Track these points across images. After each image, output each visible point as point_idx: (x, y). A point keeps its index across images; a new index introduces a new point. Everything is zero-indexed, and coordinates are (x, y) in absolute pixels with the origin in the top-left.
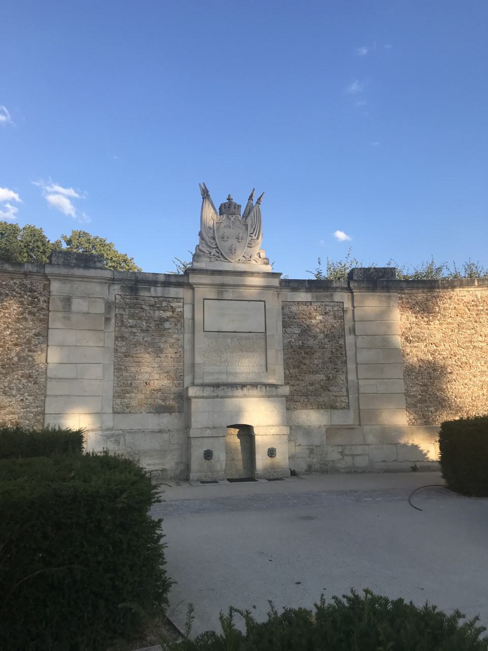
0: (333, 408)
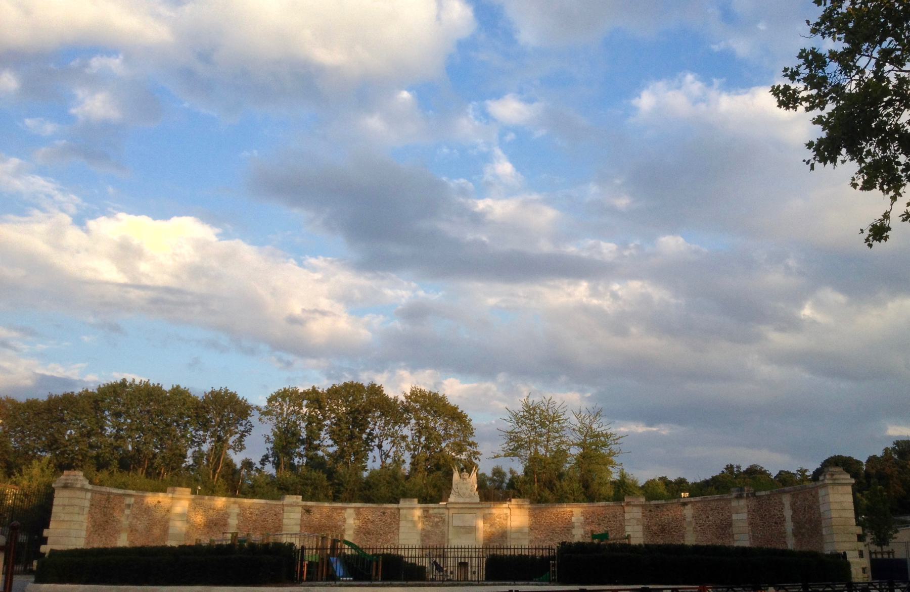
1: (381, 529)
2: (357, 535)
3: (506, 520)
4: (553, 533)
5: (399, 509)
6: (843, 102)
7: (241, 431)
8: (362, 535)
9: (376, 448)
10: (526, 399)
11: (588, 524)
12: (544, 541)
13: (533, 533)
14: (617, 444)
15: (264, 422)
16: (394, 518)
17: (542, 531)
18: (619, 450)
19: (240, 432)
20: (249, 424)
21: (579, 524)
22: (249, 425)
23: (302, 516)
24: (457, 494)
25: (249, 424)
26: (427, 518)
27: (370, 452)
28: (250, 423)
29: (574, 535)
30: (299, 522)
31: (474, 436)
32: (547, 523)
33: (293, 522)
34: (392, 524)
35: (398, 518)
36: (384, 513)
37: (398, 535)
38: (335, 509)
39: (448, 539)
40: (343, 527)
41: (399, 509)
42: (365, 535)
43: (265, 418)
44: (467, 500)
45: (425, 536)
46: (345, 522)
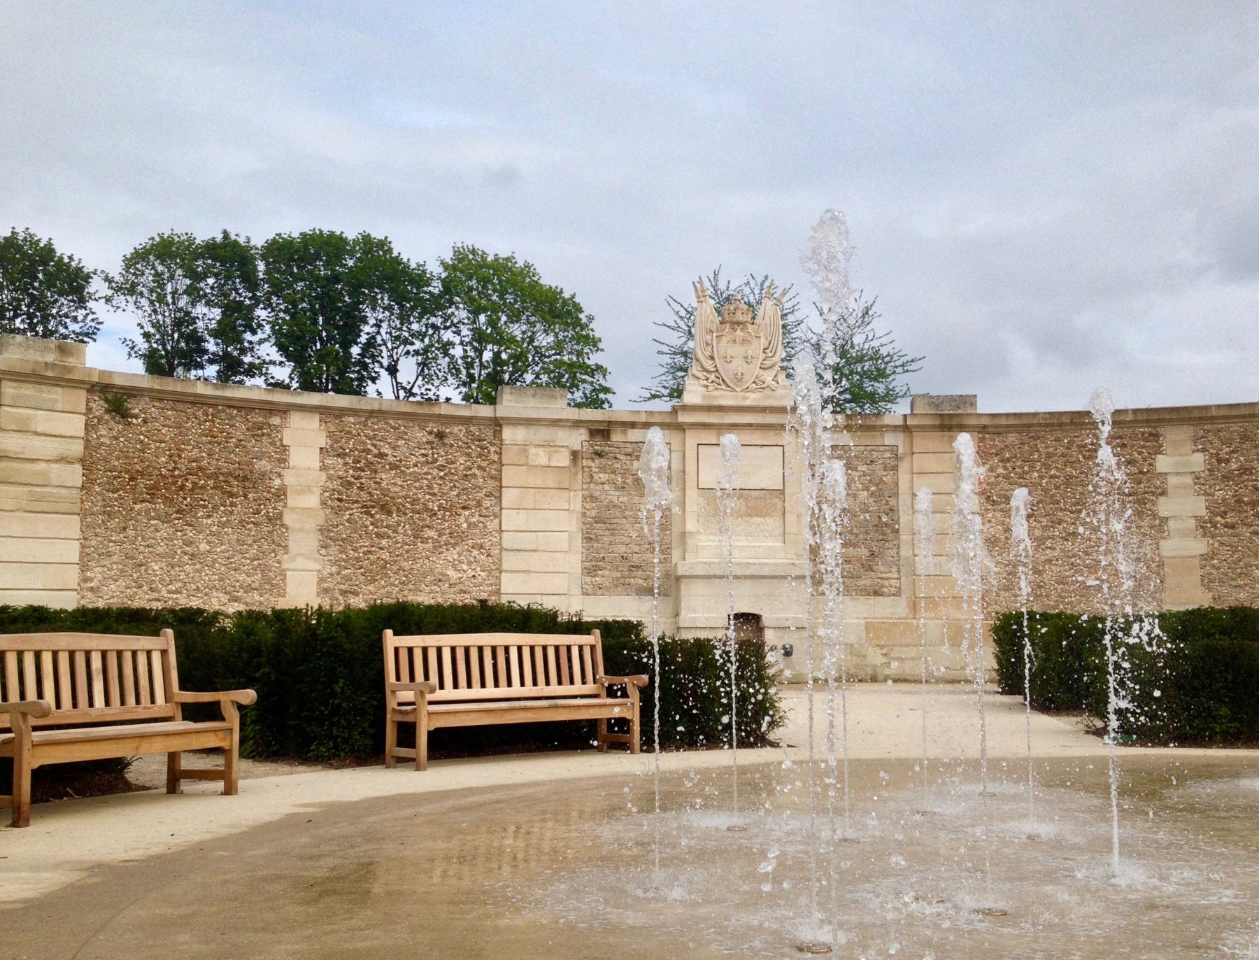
0: (876, 593)
1: (434, 495)
2: (338, 511)
3: (895, 468)
5: (497, 424)
6: (248, 696)
7: (74, 332)
8: (356, 512)
9: (384, 373)
10: (712, 279)
11: (1226, 478)
13: (999, 515)
14: (907, 371)
15: (118, 307)
16: (480, 455)
18: (905, 388)
19: (73, 336)
20: (91, 317)
21: (1189, 480)
22: (93, 320)
23: (88, 427)
24: (712, 377)
25: (91, 317)
26: (603, 461)
27: (370, 382)
28: (93, 313)
30: (77, 448)
31: (602, 350)
32: (1052, 477)
33: (50, 448)
34: (474, 476)
35: (496, 458)
36: (441, 436)
37: (498, 516)
38: (239, 408)
39: (683, 535)
40: (277, 482)
41: (497, 424)
42: (368, 513)
43: (120, 299)
44: (752, 399)
45: (598, 520)
46: (283, 461)
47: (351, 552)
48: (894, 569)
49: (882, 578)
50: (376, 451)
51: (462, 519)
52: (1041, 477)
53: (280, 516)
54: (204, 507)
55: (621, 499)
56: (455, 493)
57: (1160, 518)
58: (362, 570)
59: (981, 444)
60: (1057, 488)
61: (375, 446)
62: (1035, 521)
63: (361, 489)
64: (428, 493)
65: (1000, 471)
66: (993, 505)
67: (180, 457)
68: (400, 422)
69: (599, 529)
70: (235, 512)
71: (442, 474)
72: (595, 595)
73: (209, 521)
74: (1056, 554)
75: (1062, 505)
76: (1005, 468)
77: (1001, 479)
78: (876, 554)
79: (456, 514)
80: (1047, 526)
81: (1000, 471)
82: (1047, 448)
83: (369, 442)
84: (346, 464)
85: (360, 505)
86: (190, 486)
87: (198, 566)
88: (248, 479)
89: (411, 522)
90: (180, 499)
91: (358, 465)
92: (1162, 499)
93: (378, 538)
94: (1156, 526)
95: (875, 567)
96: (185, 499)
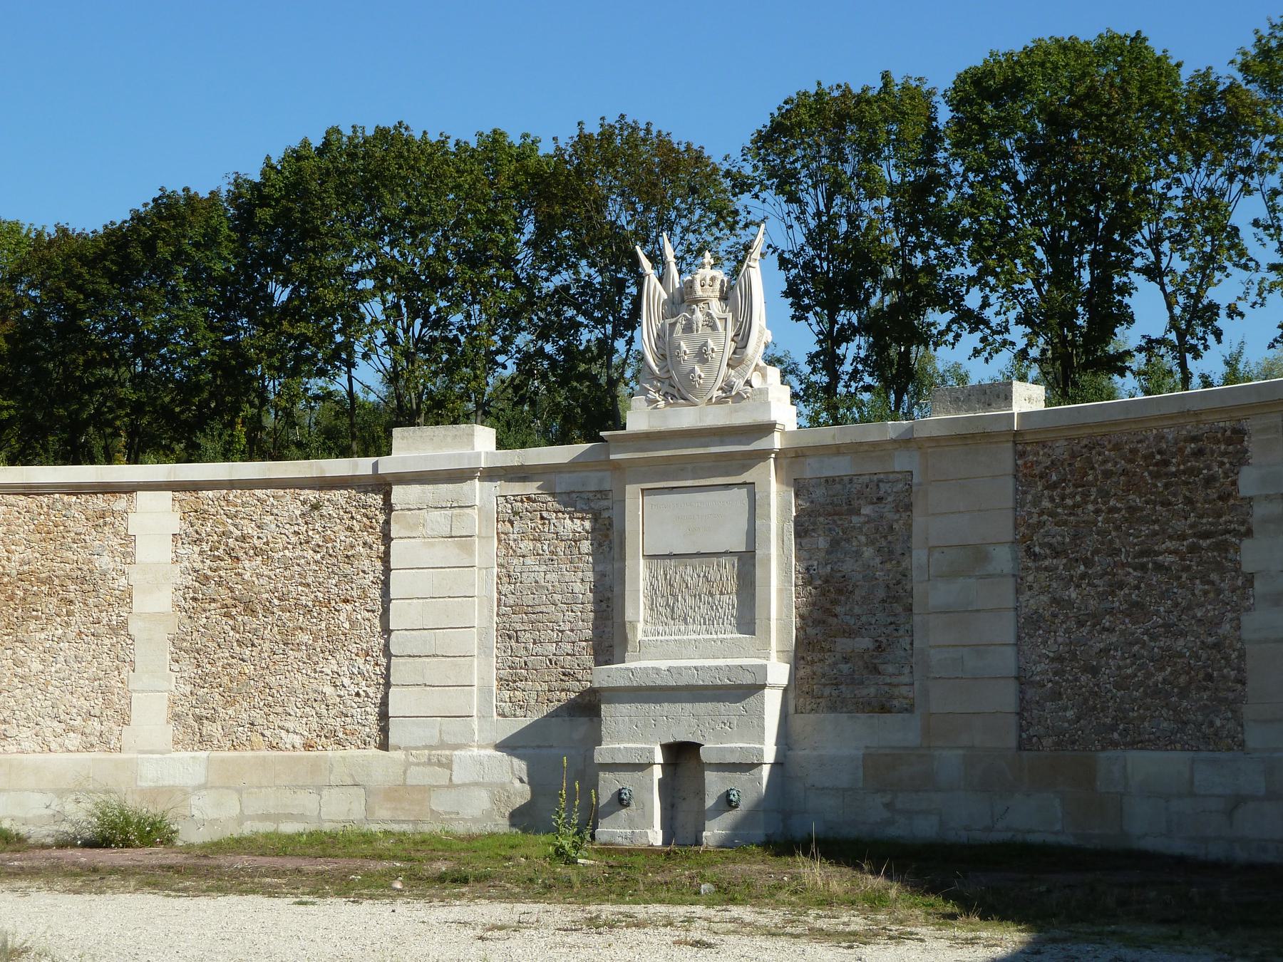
0: (884, 709)
1: (308, 585)
3: (909, 507)
4: (1143, 567)
5: (382, 485)
12: (1096, 618)
17: (1088, 563)
29: (1250, 579)
32: (1113, 510)
41: (382, 485)
42: (227, 615)
47: (208, 666)
48: (906, 670)
49: (890, 684)
50: (239, 533)
51: (343, 616)
52: (1097, 512)
53: (124, 625)
54: (37, 618)
55: (548, 577)
56: (334, 582)
57: (1245, 575)
58: (221, 689)
59: (1019, 462)
60: (1118, 528)
61: (235, 526)
62: (1089, 584)
63: (219, 584)
64: (301, 584)
65: (1046, 504)
66: (1034, 561)
67: (9, 559)
68: (268, 492)
69: (517, 621)
70: (73, 622)
71: (318, 557)
72: (515, 716)
73: (43, 636)
74: (1114, 639)
75: (1123, 557)
76: (1052, 499)
77: (1045, 517)
78: (884, 645)
79: (336, 610)
80: (1104, 592)
81: (1046, 504)
82: (1105, 462)
83: (230, 521)
84: (201, 552)
85: (219, 605)
86: (22, 594)
87: (30, 690)
88: (87, 581)
89: (279, 623)
90: (11, 611)
91: (216, 553)
92: (1247, 543)
93: (240, 646)
94: (1239, 588)
95: (881, 667)
96: (15, 610)
